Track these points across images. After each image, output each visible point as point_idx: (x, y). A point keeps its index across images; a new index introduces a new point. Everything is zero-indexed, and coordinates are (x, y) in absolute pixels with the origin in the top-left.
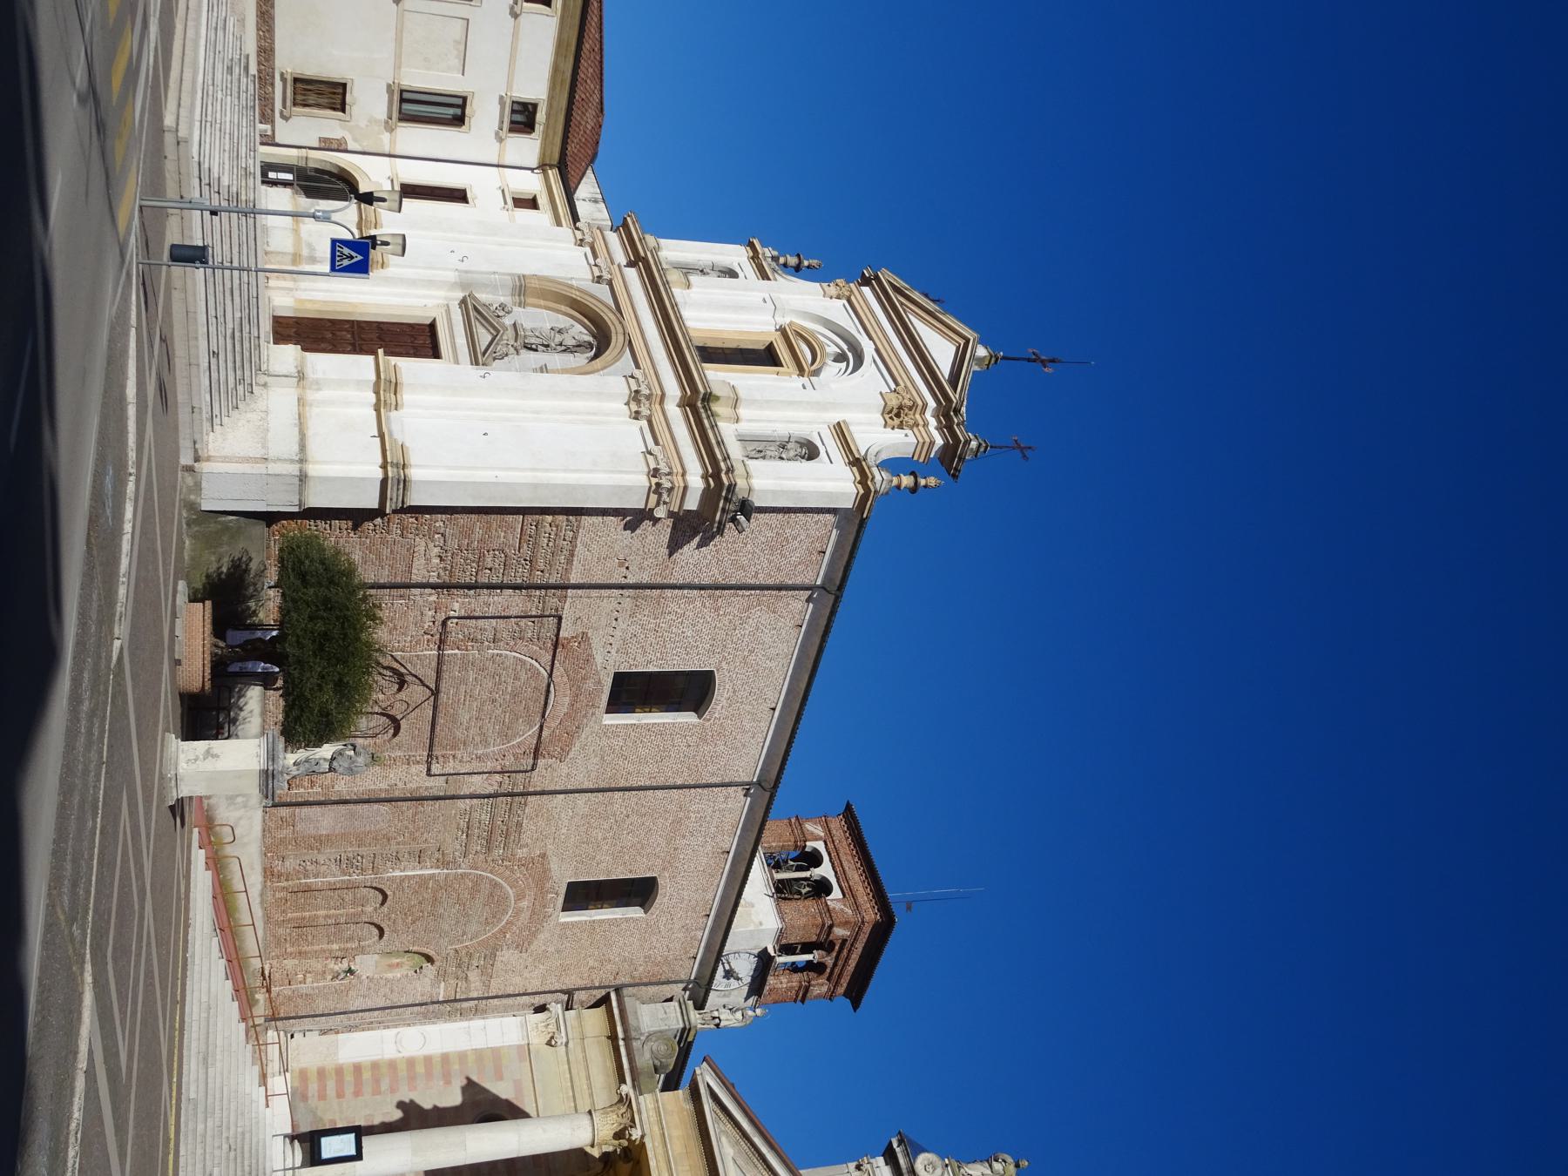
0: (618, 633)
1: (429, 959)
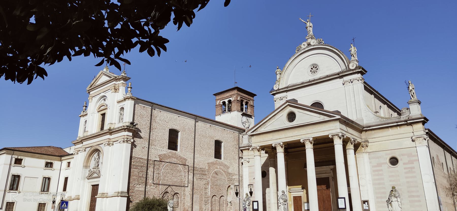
0: (159, 149)
1: (229, 186)
